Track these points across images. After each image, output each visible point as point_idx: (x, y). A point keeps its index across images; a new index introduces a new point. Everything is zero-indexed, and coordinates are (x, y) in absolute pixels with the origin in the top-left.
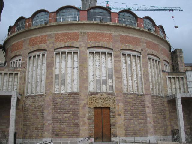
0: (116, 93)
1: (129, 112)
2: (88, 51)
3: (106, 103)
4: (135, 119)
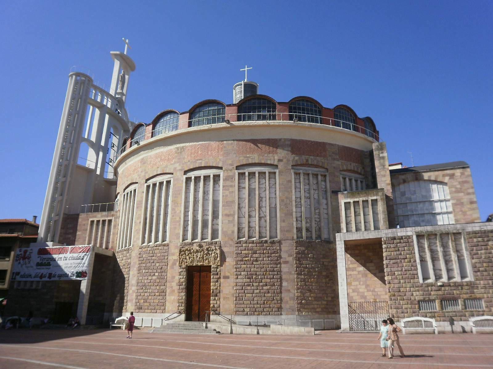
0: (223, 241)
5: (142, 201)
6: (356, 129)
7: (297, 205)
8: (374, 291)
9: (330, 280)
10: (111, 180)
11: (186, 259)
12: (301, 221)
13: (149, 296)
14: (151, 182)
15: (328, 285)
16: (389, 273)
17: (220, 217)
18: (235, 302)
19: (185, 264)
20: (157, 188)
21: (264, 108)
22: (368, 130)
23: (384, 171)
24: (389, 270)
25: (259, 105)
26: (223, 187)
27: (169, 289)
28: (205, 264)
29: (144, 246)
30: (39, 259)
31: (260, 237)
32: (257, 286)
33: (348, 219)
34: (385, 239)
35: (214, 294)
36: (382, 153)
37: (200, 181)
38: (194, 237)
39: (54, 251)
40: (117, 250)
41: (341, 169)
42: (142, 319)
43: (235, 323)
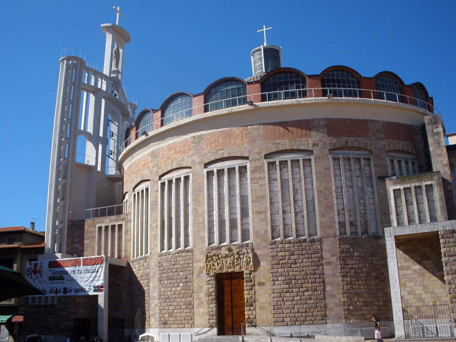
4: (294, 290)
5: (157, 201)
6: (403, 100)
7: (338, 196)
8: (432, 292)
9: (381, 281)
10: (114, 176)
11: (214, 265)
12: (344, 215)
13: (175, 309)
14: (165, 178)
15: (378, 287)
16: (449, 272)
17: (250, 215)
18: (273, 311)
19: (214, 271)
20: (173, 186)
21: (292, 83)
22: (418, 99)
23: (439, 149)
24: (448, 268)
25: (286, 80)
26: (251, 179)
27: (197, 300)
28: (236, 270)
29: (164, 253)
30: (51, 272)
31: (298, 236)
32: (297, 292)
33: (398, 208)
34: (443, 232)
35: (248, 303)
36: (437, 127)
37: (223, 174)
38: (222, 239)
39: (65, 263)
40: (132, 259)
41: (388, 150)
42: (169, 335)
43: (274, 335)
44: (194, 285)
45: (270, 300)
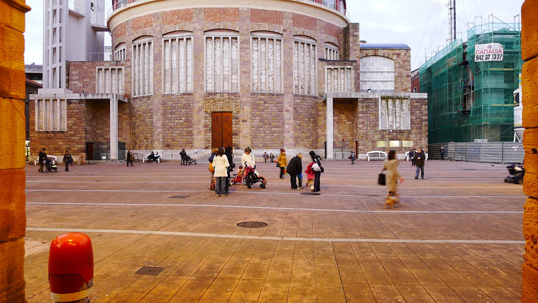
1: (257, 118)
2: (205, 37)
3: (227, 106)
4: (266, 126)
44: (194, 119)
45: (250, 132)
